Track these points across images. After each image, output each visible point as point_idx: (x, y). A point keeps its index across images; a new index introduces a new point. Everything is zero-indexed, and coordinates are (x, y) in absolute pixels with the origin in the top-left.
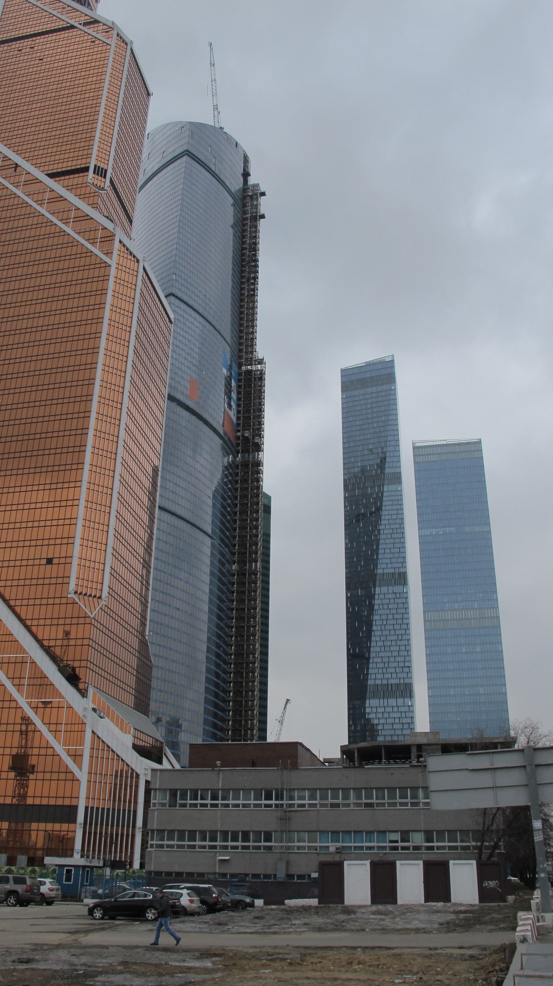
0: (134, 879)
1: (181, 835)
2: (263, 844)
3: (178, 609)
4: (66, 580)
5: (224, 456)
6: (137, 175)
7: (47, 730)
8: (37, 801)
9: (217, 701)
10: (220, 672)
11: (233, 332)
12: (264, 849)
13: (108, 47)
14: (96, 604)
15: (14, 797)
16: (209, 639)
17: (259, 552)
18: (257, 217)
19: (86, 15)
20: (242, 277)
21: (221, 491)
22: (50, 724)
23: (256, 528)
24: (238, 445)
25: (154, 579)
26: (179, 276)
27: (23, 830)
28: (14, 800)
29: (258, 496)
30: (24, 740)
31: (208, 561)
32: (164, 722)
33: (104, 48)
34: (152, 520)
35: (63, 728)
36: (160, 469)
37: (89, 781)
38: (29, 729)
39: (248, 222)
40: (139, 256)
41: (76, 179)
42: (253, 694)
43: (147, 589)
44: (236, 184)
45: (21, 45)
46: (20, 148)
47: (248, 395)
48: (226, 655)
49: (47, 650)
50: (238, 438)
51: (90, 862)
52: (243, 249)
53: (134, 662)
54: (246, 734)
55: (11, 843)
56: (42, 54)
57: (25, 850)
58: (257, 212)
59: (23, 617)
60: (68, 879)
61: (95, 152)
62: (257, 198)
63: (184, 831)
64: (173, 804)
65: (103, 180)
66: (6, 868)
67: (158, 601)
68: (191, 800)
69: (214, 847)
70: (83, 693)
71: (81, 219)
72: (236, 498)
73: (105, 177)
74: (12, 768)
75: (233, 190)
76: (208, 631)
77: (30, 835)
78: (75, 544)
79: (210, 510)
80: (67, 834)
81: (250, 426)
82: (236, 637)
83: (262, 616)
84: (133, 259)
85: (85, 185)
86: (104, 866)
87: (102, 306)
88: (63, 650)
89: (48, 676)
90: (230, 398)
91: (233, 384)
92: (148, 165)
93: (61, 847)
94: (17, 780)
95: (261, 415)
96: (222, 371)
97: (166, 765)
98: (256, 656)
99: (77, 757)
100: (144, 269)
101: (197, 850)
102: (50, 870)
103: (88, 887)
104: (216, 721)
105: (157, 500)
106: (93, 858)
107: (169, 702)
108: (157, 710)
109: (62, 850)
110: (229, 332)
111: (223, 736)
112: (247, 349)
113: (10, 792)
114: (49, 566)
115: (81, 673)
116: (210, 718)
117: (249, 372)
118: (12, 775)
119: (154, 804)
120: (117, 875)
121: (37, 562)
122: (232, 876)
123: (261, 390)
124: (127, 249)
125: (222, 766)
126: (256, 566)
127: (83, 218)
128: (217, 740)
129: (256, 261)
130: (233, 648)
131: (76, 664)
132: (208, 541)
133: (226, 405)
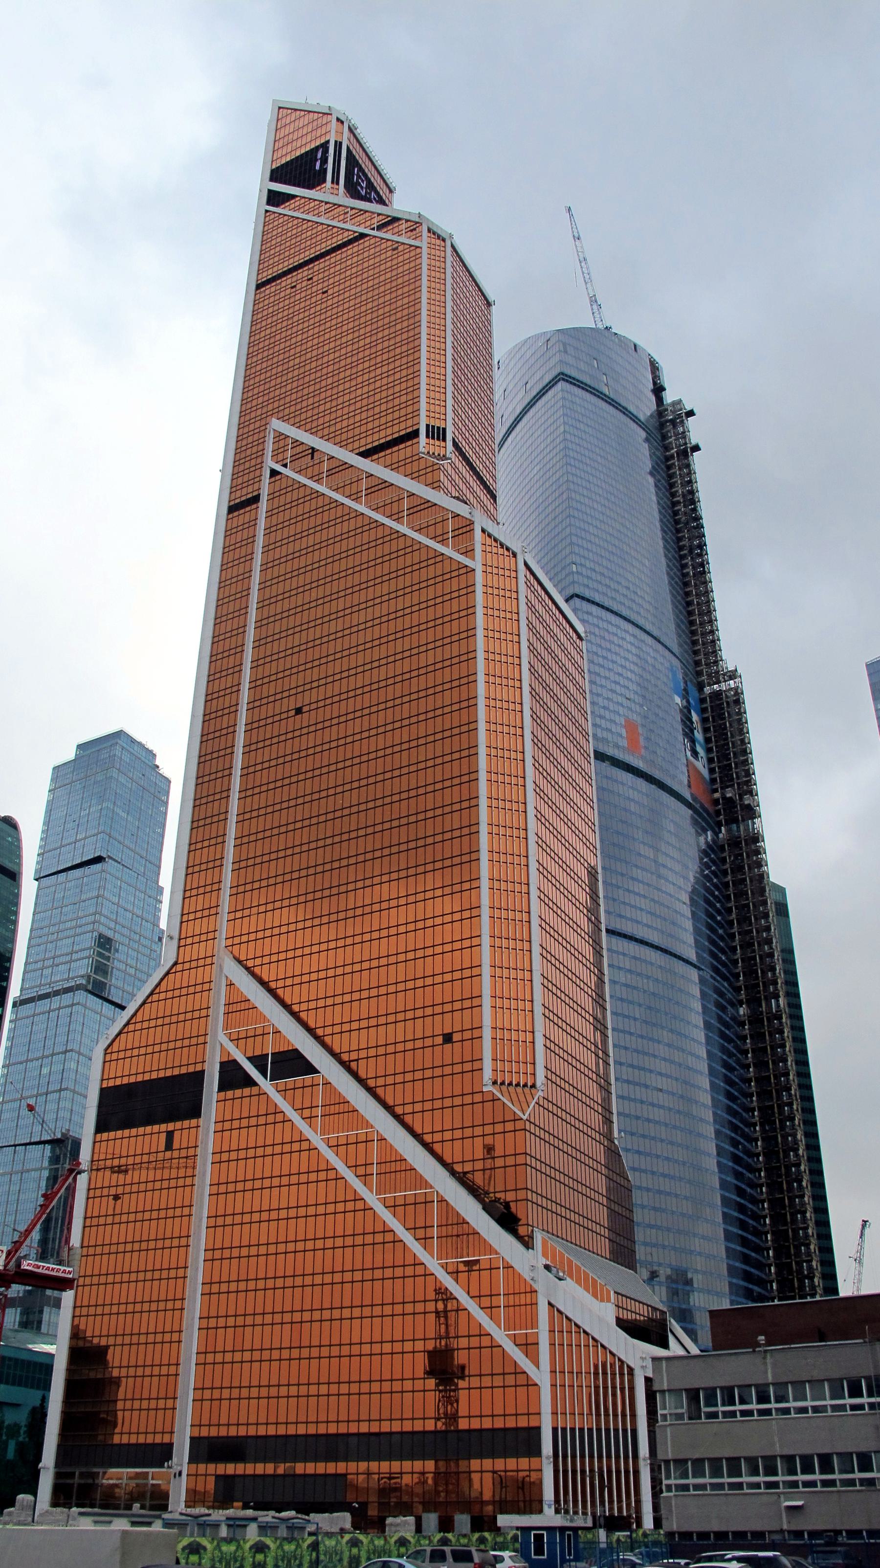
0: (647, 1546)
1: (716, 1466)
2: (858, 1475)
3: (661, 1090)
4: (476, 1065)
5: (698, 834)
6: (492, 425)
7: (477, 1307)
8: (475, 1424)
9: (745, 1234)
10: (743, 1186)
11: (679, 636)
12: (861, 1485)
13: (418, 250)
14: (529, 1097)
15: (438, 1419)
16: (718, 1133)
17: (779, 981)
18: (688, 451)
19: (379, 215)
20: (681, 548)
21: (703, 891)
22: (480, 1297)
23: (769, 942)
24: (718, 813)
25: (615, 1046)
26: (581, 565)
27: (458, 1473)
28: (439, 1424)
29: (762, 891)
30: (443, 1326)
31: (697, 1006)
32: (662, 1278)
33: (413, 254)
34: (598, 953)
35: (502, 1300)
36: (600, 870)
37: (553, 1385)
38: (449, 1308)
39: (675, 461)
40: (515, 546)
41: (403, 451)
42: (804, 1217)
43: (606, 1063)
44: (646, 408)
45: (294, 279)
46: (344, 436)
47: (721, 733)
48: (749, 1157)
49: (462, 1179)
50: (716, 802)
51: (572, 1520)
52: (674, 504)
53: (602, 1185)
54: (802, 1286)
55: (443, 1494)
56: (326, 284)
57: (466, 1505)
58: (686, 444)
59: (418, 1130)
60: (539, 1551)
61: (423, 406)
62: (682, 422)
63: (720, 1460)
64: (695, 1414)
65: (443, 444)
66: (439, 1536)
67: (628, 1082)
68: (723, 1405)
69: (775, 1485)
70: (527, 1243)
71: (419, 508)
72: (728, 898)
73: (444, 440)
74: (430, 1372)
75: (642, 418)
76: (715, 1121)
77: (470, 1480)
78: (484, 1007)
79: (689, 925)
80: (529, 1476)
81: (732, 779)
82: (762, 1125)
83: (800, 1086)
84: (506, 553)
85: (416, 457)
86: (595, 1526)
87: (471, 633)
88: (487, 1177)
89: (468, 1219)
90: (693, 741)
91: (695, 717)
92: (505, 407)
93: (521, 1498)
94: (440, 1391)
95: (747, 760)
96: (673, 700)
97: (675, 1349)
98: (801, 1152)
99: (529, 1346)
100: (526, 564)
101: (746, 1491)
102: (509, 1537)
103: (573, 1564)
104: (748, 1268)
105: (603, 920)
106: (576, 1513)
107: (666, 1243)
108: (649, 1258)
109: (524, 1502)
110: (675, 637)
111: (763, 1292)
112: (707, 659)
113: (431, 1412)
114: (448, 1046)
115: (518, 1210)
116: (738, 1264)
117: (717, 695)
118: (431, 1383)
119: (664, 1417)
120: (618, 1540)
121: (428, 1042)
122: (813, 1534)
123: (740, 720)
124: (496, 540)
125: (769, 1343)
126: (778, 1006)
127: (422, 507)
128: (754, 1301)
129: (698, 518)
130: (759, 1143)
131: (510, 1196)
132: (694, 974)
133: (689, 753)
